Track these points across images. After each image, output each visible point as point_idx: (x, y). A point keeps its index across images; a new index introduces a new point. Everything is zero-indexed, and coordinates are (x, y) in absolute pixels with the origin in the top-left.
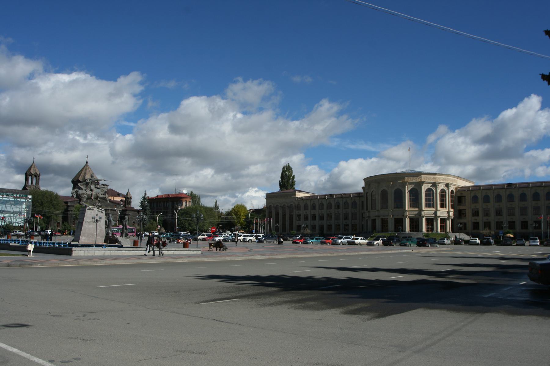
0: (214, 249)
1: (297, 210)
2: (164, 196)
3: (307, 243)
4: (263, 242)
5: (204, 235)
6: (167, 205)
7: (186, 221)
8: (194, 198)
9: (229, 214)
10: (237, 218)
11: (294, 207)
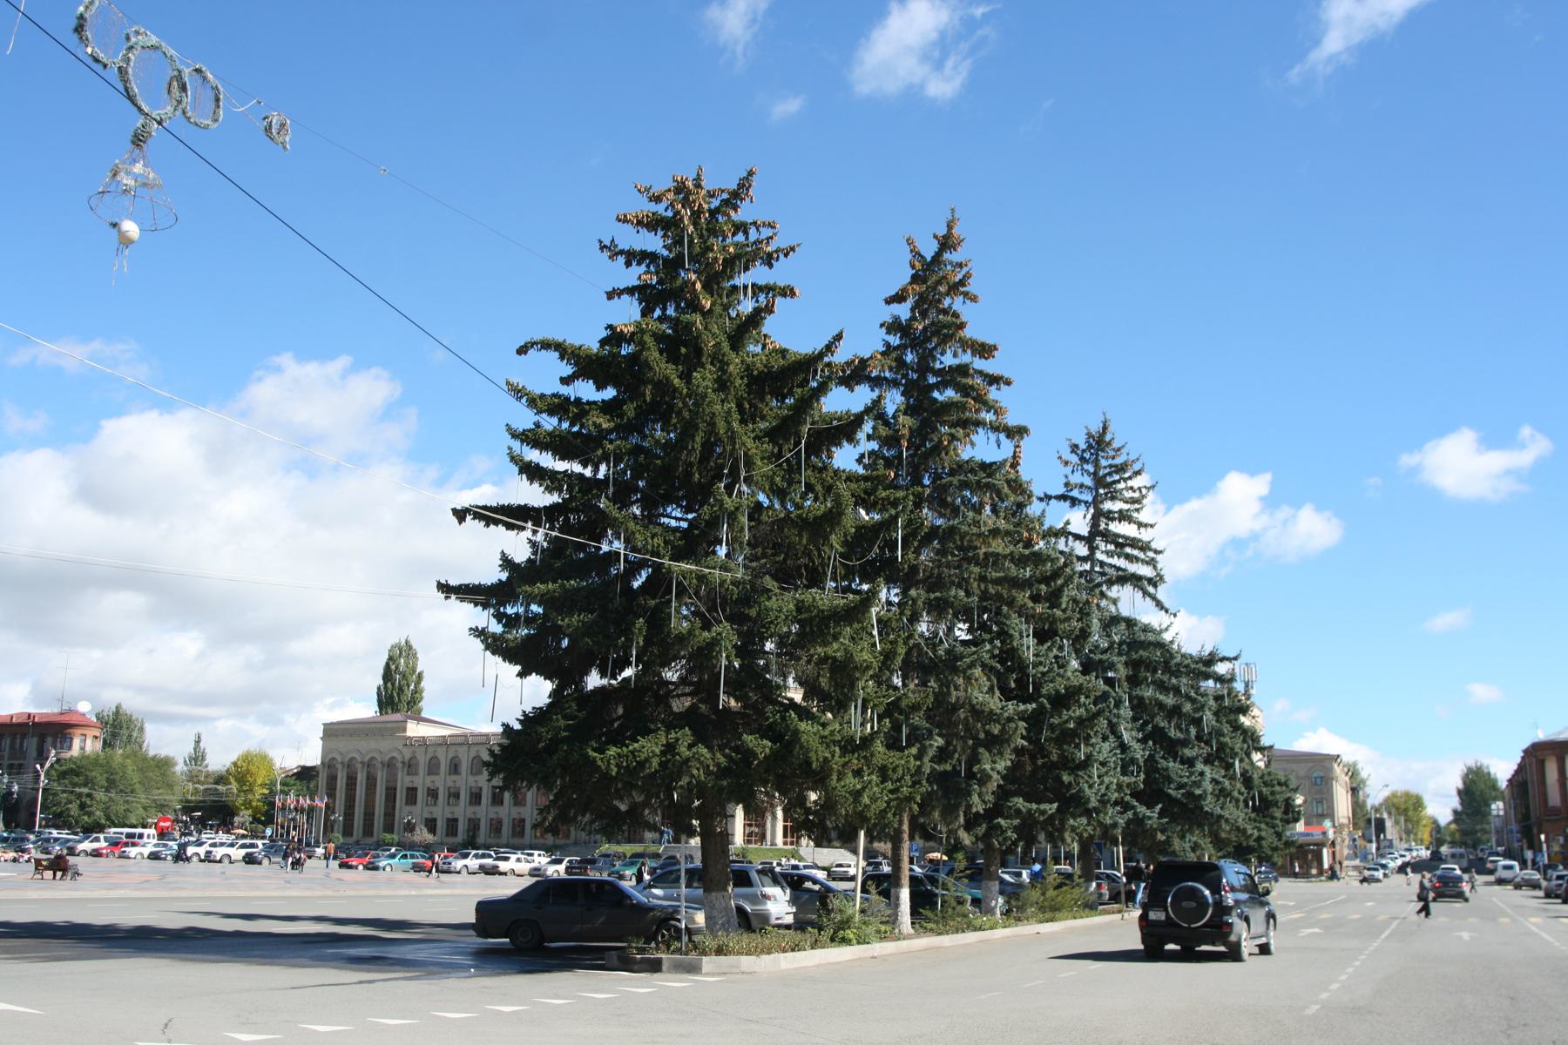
0: (49, 874)
1: (408, 774)
2: (17, 718)
3: (376, 868)
4: (260, 863)
5: (97, 840)
6: (22, 745)
7: (73, 798)
8: (118, 727)
9: (221, 779)
10: (244, 791)
11: (379, 766)
